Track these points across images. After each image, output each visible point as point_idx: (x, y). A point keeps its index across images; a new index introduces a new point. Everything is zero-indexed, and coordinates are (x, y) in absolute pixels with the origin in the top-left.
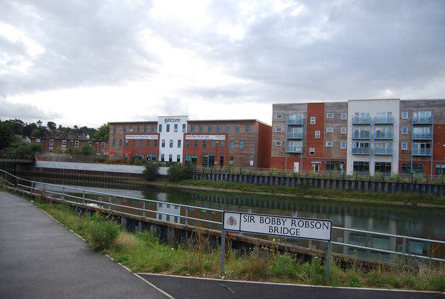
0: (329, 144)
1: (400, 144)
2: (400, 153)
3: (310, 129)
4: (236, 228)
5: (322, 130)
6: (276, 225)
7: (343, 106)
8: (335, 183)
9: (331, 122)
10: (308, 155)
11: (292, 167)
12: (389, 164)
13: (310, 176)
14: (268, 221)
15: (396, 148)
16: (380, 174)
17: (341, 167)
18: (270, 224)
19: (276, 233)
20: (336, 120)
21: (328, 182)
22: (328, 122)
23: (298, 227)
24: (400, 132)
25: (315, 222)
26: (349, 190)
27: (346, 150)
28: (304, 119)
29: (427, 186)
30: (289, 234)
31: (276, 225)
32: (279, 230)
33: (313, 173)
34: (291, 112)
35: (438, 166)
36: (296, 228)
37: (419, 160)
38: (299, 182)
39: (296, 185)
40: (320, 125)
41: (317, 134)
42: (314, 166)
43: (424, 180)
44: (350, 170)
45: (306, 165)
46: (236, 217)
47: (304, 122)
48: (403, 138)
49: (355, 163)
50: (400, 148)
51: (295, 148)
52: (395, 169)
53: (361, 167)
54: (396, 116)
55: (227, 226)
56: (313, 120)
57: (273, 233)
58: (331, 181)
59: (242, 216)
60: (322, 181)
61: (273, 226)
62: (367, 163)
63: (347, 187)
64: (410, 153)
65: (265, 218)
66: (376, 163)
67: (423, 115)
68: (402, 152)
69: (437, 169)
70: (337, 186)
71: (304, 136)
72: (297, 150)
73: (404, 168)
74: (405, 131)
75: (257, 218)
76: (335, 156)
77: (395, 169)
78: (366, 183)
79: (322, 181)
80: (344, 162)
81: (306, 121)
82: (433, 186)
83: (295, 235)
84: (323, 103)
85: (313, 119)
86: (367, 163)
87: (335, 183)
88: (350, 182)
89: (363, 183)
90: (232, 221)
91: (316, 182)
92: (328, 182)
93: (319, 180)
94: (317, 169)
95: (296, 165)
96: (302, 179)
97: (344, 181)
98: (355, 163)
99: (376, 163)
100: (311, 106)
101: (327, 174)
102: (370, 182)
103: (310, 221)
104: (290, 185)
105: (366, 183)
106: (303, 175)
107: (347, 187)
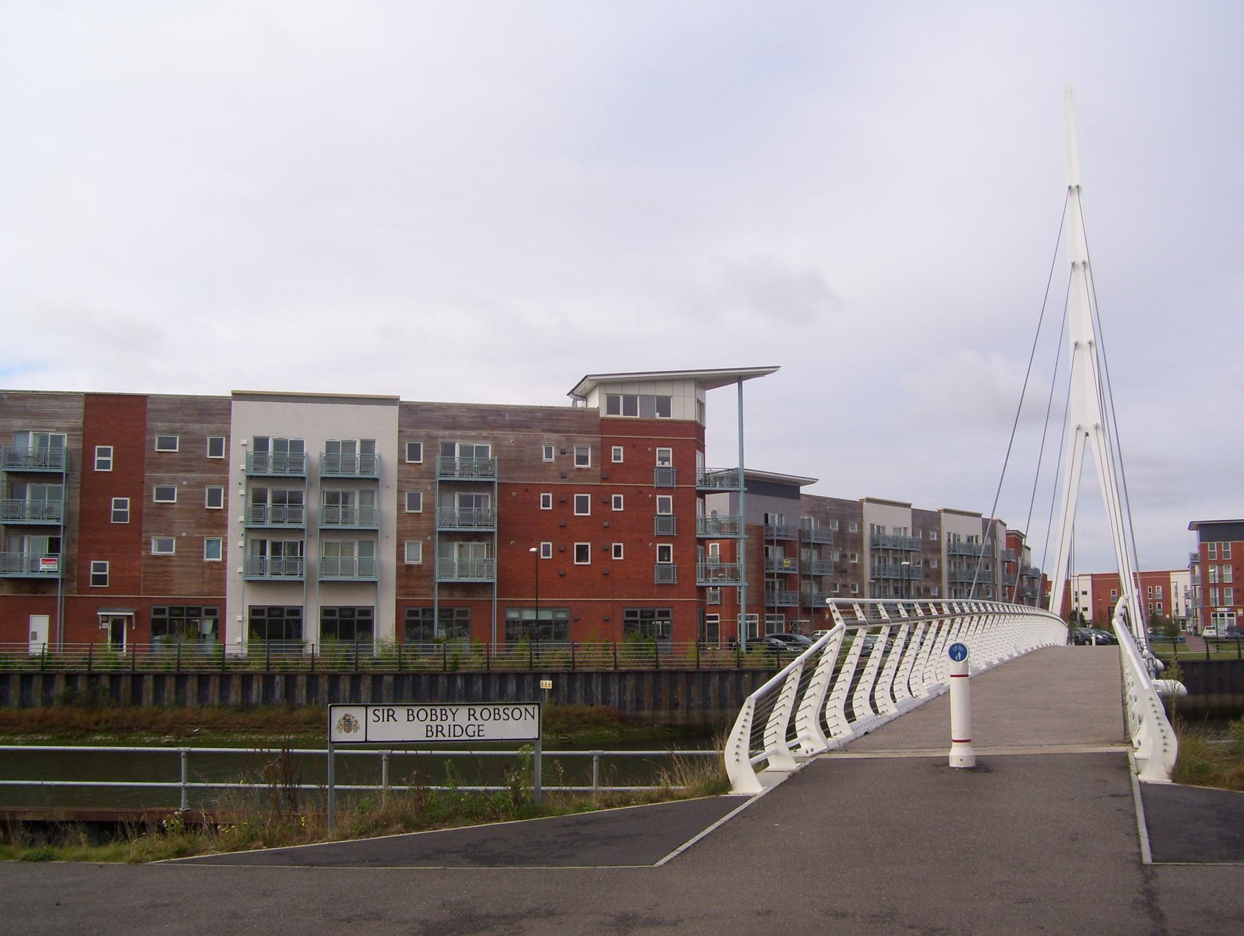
0: (164, 546)
1: (400, 546)
2: (399, 576)
3: (94, 488)
4: (358, 736)
5: (138, 494)
6: (438, 722)
7: (213, 411)
8: (192, 685)
9: (170, 466)
10: (83, 587)
11: (24, 635)
12: (368, 612)
13: (99, 664)
14: (422, 715)
15: (386, 555)
16: (341, 648)
17: (208, 627)
18: (428, 722)
19: (440, 737)
20: (188, 463)
21: (170, 684)
22: (158, 466)
23: (480, 722)
24: (400, 507)
25: (511, 708)
26: (246, 706)
27: (222, 566)
28: (70, 453)
29: (486, 676)
30: (464, 737)
31: (438, 722)
32: (446, 731)
33: (114, 654)
34: (18, 423)
35: (513, 615)
36: (476, 723)
37: (458, 596)
38: (60, 687)
39: (47, 702)
40: (131, 473)
41: (120, 506)
42: (108, 626)
43: (475, 662)
44: (237, 639)
45: (75, 623)
46: (357, 713)
47: (70, 465)
48: (410, 524)
49: (255, 611)
50: (400, 556)
51: (34, 562)
52: (385, 626)
53: (273, 626)
54: (388, 451)
55: (338, 735)
56: (105, 458)
57: (434, 738)
58: (181, 678)
59: (370, 710)
60: (149, 683)
61: (434, 724)
62: (296, 611)
63: (234, 697)
64: (430, 574)
65: (416, 709)
66: (326, 611)
67: (471, 454)
68: (406, 573)
69: (514, 623)
70: (202, 697)
71: (69, 515)
72: (43, 567)
73: (412, 622)
74: (414, 502)
75: (401, 713)
76: (185, 588)
77: (385, 626)
78: (302, 680)
79: (149, 683)
80: (216, 612)
81: (78, 460)
82: (503, 676)
83: (476, 738)
84: (142, 399)
85: (104, 464)
86: (296, 611)
87: (192, 685)
88: (247, 679)
89: (290, 679)
90: (348, 724)
91: (125, 684)
92: (170, 684)
93: (137, 678)
94: (117, 637)
95: (40, 625)
96: (71, 678)
97: (225, 674)
98: (255, 611)
99: (326, 611)
100: (95, 402)
101: (161, 653)
102: (312, 678)
103: (501, 708)
104: (25, 703)
105: (302, 680)
106: (73, 658)
107: (234, 697)
